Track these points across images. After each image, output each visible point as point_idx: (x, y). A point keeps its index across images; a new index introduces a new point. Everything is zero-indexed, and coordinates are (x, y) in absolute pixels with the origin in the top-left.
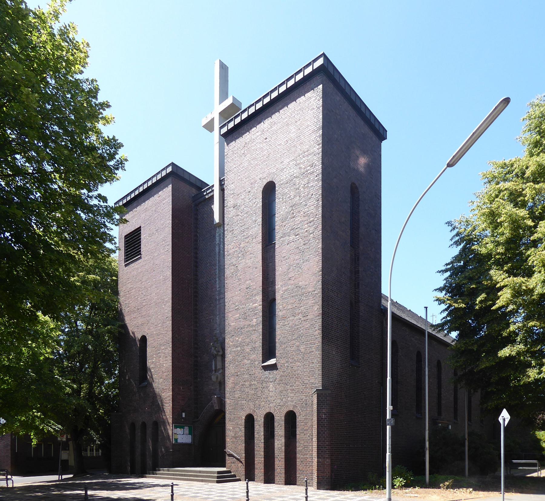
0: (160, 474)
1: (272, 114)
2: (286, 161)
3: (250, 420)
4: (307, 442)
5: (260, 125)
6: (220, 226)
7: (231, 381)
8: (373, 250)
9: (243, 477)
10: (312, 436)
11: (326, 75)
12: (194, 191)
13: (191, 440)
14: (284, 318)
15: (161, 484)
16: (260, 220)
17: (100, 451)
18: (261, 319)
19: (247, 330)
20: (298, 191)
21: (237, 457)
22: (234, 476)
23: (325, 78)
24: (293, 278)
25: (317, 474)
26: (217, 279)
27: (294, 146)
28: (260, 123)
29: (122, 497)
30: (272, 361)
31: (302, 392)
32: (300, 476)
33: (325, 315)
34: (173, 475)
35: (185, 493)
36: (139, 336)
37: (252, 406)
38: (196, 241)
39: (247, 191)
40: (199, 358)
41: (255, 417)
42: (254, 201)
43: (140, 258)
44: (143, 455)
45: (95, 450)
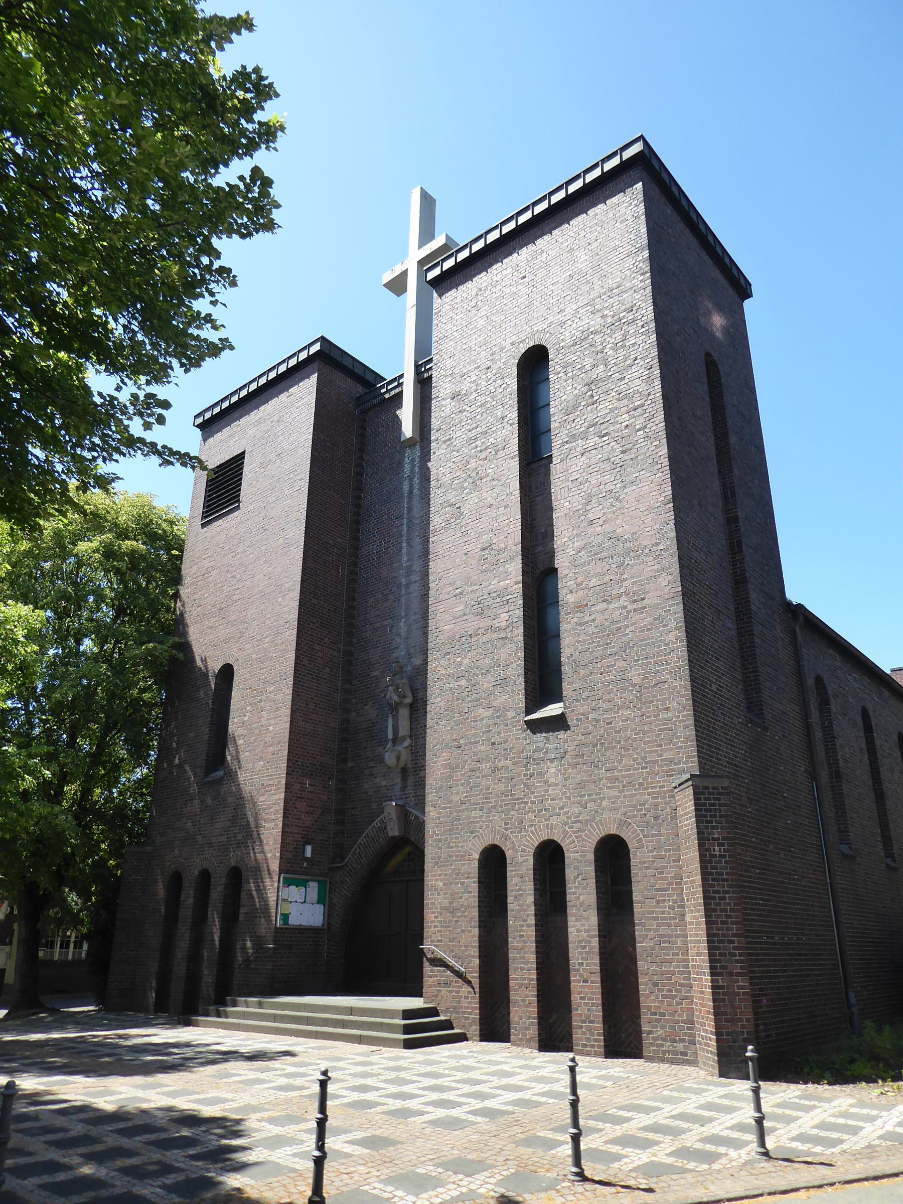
0: (244, 1016)
1: (537, 238)
2: (570, 309)
3: (493, 863)
4: (669, 925)
5: (510, 258)
6: (414, 445)
7: (441, 761)
8: (756, 482)
9: (474, 1030)
10: (683, 906)
11: (643, 168)
12: (360, 389)
13: (321, 918)
14: (581, 607)
15: (243, 1050)
16: (513, 415)
17: (85, 946)
18: (520, 613)
19: (485, 639)
20: (600, 355)
21: (458, 967)
22: (448, 1025)
23: (645, 174)
24: (601, 522)
25: (717, 1027)
26: (404, 545)
27: (588, 282)
28: (510, 254)
29: (131, 1107)
30: (553, 710)
31: (640, 784)
32: (651, 1028)
33: (689, 596)
34: (275, 1018)
35: (243, 1043)
36: (215, 666)
37: (499, 826)
38: (360, 474)
39: (482, 367)
40: (354, 714)
41: (508, 854)
42: (499, 382)
43: (238, 508)
44: (194, 958)
45: (72, 945)
